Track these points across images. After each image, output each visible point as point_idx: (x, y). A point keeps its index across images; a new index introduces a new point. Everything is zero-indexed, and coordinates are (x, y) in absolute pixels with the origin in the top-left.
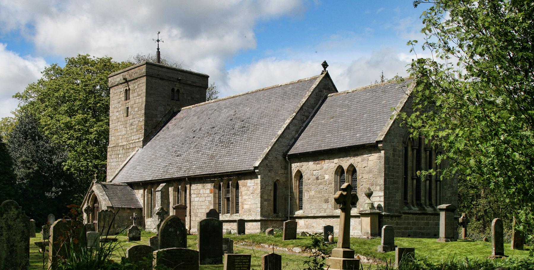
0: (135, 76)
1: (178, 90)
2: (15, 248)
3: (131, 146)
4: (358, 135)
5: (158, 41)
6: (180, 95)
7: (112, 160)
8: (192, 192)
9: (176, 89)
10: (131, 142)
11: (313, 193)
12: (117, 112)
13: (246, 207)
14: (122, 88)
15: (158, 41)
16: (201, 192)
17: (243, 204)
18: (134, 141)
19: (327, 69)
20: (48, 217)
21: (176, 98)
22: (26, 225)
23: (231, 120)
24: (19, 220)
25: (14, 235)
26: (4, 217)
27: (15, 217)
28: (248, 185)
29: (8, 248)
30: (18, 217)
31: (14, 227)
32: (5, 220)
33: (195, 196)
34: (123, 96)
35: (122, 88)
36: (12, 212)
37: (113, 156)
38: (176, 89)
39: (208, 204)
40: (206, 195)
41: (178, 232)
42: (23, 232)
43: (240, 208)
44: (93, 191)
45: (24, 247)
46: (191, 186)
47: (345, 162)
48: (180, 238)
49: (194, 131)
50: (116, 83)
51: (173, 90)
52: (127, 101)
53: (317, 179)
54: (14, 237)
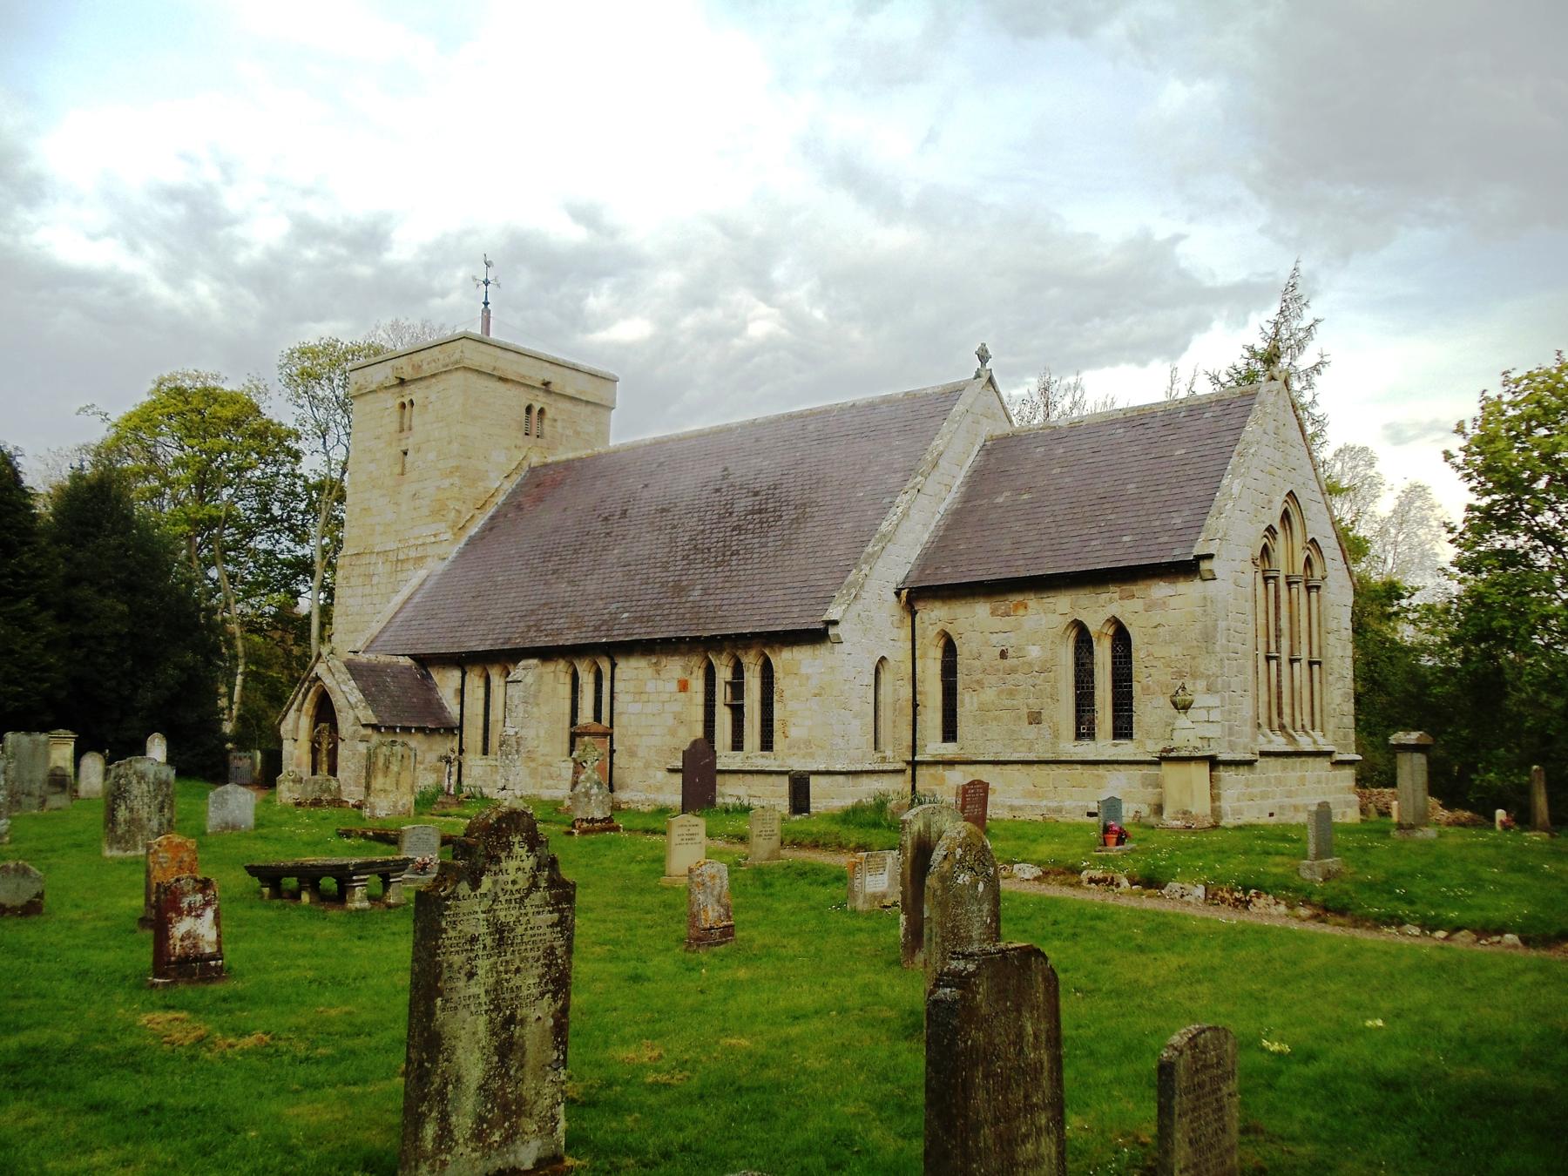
0: (427, 370)
1: (542, 411)
2: (517, 1031)
3: (413, 554)
4: (1125, 539)
5: (487, 283)
6: (546, 422)
7: (349, 592)
8: (618, 686)
9: (537, 408)
10: (412, 542)
11: (989, 695)
12: (372, 461)
13: (794, 732)
14: (391, 400)
15: (487, 283)
16: (650, 686)
17: (784, 724)
18: (420, 541)
19: (988, 366)
20: (149, 744)
21: (534, 431)
22: (560, 922)
23: (717, 490)
24: (537, 897)
25: (518, 970)
26: (483, 890)
27: (523, 884)
28: (803, 671)
29: (494, 1034)
30: (534, 886)
31: (520, 930)
32: (487, 902)
33: (629, 698)
34: (391, 421)
35: (391, 400)
36: (511, 865)
37: (353, 581)
38: (537, 408)
39: (670, 721)
40: (666, 697)
41: (981, 887)
42: (551, 951)
43: (777, 736)
44: (318, 678)
45: (551, 1022)
46: (613, 666)
47: (1096, 609)
48: (986, 907)
49: (606, 519)
50: (374, 387)
51: (529, 409)
52: (404, 434)
53: (1003, 655)
54: (516, 981)
